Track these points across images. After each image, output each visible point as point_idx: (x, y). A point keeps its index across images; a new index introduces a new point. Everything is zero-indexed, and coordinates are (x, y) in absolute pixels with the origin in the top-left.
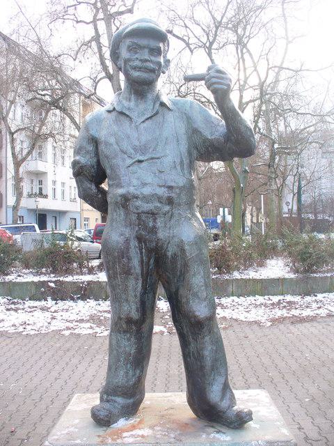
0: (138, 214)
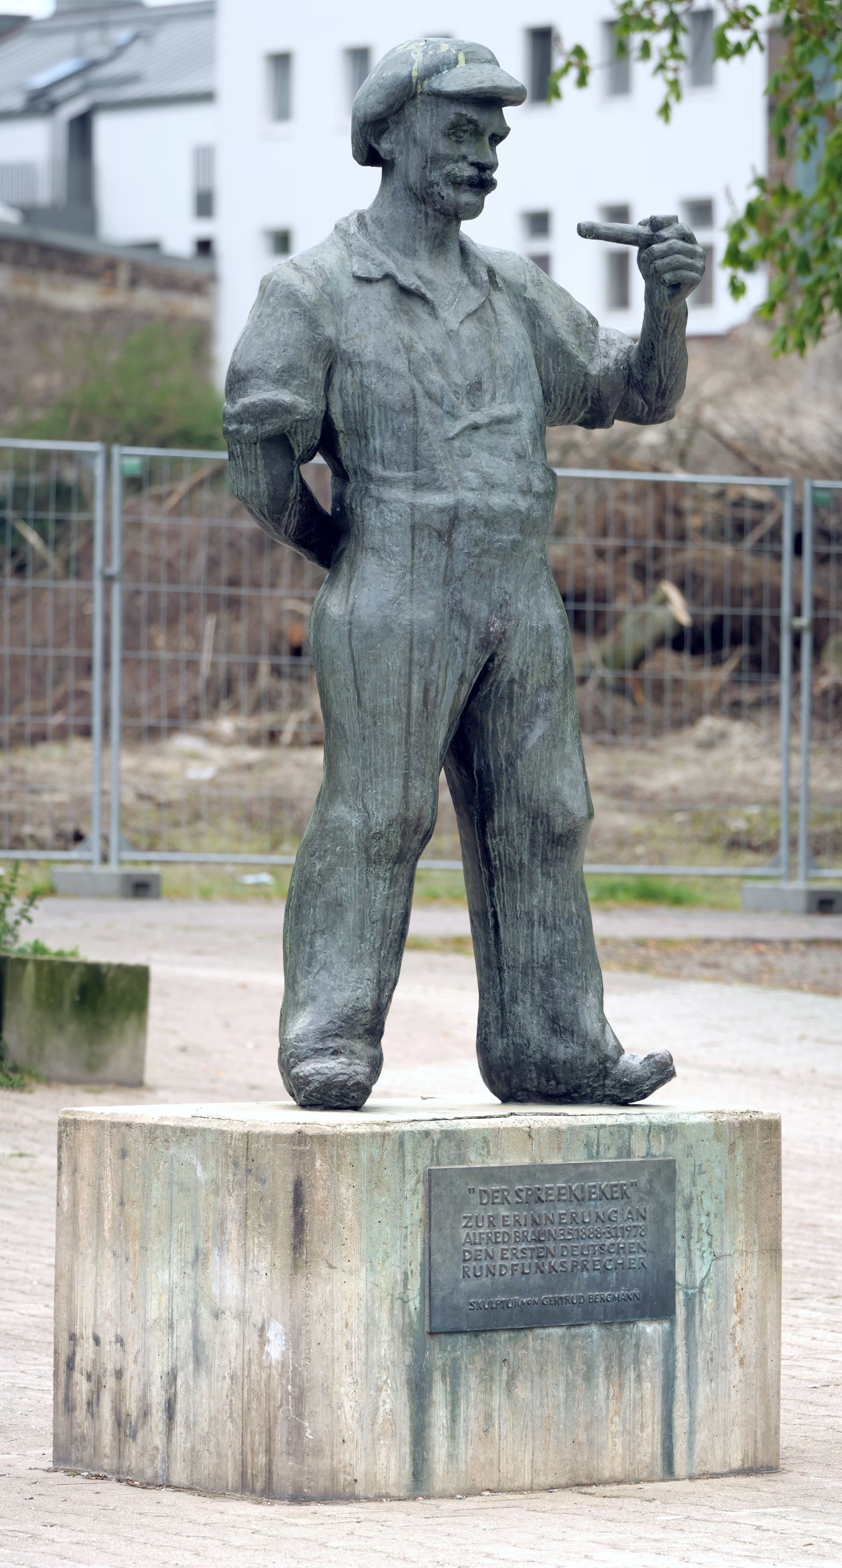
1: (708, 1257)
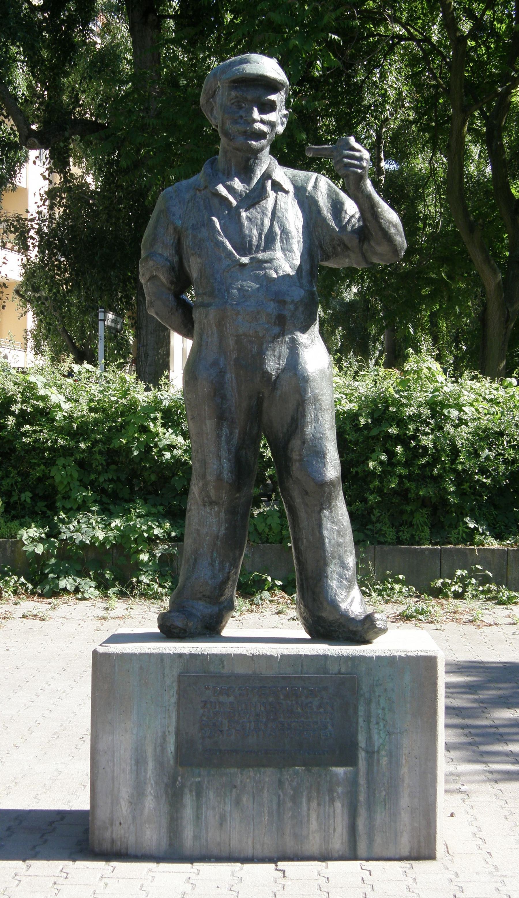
1: (383, 735)
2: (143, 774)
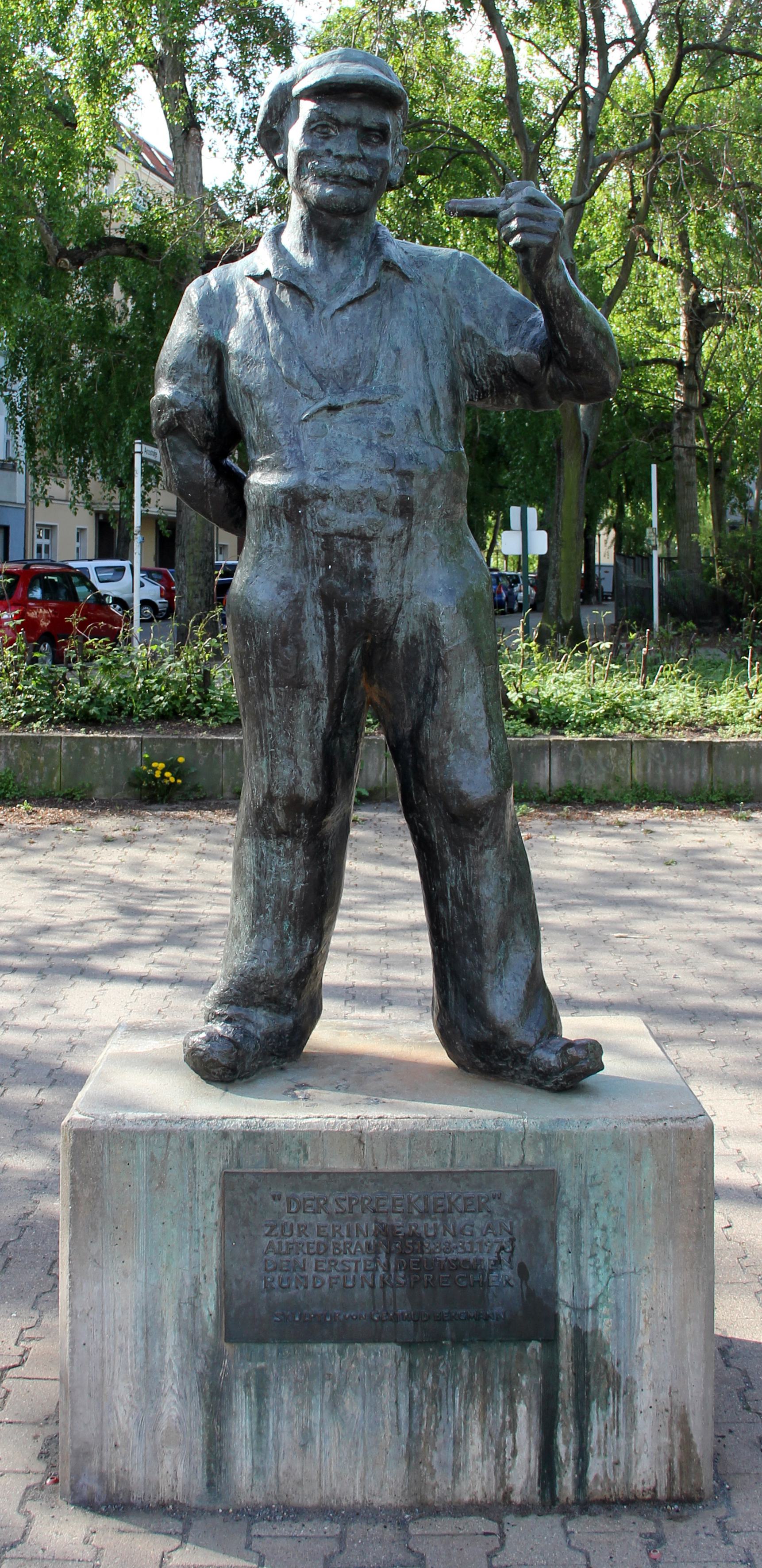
0: (326, 536)
1: (603, 1275)
2: (158, 1354)
